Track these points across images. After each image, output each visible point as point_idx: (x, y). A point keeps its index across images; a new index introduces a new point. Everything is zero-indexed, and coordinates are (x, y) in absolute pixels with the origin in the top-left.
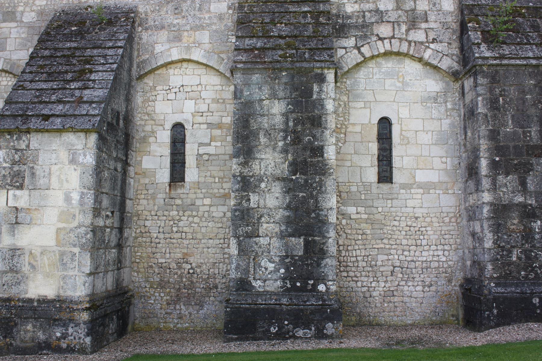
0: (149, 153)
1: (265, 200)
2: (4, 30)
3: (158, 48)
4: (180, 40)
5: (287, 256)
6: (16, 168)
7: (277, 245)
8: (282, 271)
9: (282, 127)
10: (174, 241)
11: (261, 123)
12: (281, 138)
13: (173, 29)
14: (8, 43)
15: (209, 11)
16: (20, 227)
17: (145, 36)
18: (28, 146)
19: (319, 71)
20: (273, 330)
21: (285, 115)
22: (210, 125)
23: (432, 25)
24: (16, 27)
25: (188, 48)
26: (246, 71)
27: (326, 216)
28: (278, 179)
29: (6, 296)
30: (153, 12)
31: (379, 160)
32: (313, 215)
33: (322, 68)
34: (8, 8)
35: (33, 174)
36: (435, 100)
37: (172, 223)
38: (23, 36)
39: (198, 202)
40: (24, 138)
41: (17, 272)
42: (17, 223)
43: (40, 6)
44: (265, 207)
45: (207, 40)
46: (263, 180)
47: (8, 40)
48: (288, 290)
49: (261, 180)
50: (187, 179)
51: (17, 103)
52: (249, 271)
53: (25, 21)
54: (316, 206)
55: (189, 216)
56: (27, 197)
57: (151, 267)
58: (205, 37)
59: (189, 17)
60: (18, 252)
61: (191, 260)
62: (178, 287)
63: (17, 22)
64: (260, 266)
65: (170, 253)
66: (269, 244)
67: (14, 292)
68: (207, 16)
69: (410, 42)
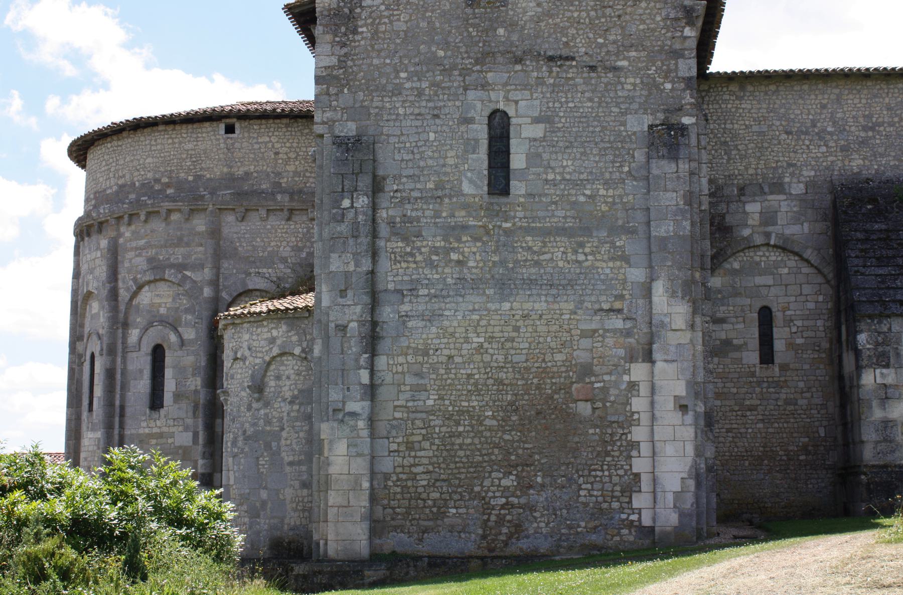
2: (773, 203)
6: (880, 349)
14: (779, 217)
16: (890, 401)
18: (890, 329)
24: (785, 200)
26: (688, 87)
29: (882, 463)
38: (795, 209)
40: (885, 322)
41: (891, 442)
42: (887, 398)
43: (809, 177)
47: (779, 214)
51: (864, 289)
53: (793, 192)
56: (893, 375)
60: (890, 424)
63: (785, 194)
67: (889, 458)
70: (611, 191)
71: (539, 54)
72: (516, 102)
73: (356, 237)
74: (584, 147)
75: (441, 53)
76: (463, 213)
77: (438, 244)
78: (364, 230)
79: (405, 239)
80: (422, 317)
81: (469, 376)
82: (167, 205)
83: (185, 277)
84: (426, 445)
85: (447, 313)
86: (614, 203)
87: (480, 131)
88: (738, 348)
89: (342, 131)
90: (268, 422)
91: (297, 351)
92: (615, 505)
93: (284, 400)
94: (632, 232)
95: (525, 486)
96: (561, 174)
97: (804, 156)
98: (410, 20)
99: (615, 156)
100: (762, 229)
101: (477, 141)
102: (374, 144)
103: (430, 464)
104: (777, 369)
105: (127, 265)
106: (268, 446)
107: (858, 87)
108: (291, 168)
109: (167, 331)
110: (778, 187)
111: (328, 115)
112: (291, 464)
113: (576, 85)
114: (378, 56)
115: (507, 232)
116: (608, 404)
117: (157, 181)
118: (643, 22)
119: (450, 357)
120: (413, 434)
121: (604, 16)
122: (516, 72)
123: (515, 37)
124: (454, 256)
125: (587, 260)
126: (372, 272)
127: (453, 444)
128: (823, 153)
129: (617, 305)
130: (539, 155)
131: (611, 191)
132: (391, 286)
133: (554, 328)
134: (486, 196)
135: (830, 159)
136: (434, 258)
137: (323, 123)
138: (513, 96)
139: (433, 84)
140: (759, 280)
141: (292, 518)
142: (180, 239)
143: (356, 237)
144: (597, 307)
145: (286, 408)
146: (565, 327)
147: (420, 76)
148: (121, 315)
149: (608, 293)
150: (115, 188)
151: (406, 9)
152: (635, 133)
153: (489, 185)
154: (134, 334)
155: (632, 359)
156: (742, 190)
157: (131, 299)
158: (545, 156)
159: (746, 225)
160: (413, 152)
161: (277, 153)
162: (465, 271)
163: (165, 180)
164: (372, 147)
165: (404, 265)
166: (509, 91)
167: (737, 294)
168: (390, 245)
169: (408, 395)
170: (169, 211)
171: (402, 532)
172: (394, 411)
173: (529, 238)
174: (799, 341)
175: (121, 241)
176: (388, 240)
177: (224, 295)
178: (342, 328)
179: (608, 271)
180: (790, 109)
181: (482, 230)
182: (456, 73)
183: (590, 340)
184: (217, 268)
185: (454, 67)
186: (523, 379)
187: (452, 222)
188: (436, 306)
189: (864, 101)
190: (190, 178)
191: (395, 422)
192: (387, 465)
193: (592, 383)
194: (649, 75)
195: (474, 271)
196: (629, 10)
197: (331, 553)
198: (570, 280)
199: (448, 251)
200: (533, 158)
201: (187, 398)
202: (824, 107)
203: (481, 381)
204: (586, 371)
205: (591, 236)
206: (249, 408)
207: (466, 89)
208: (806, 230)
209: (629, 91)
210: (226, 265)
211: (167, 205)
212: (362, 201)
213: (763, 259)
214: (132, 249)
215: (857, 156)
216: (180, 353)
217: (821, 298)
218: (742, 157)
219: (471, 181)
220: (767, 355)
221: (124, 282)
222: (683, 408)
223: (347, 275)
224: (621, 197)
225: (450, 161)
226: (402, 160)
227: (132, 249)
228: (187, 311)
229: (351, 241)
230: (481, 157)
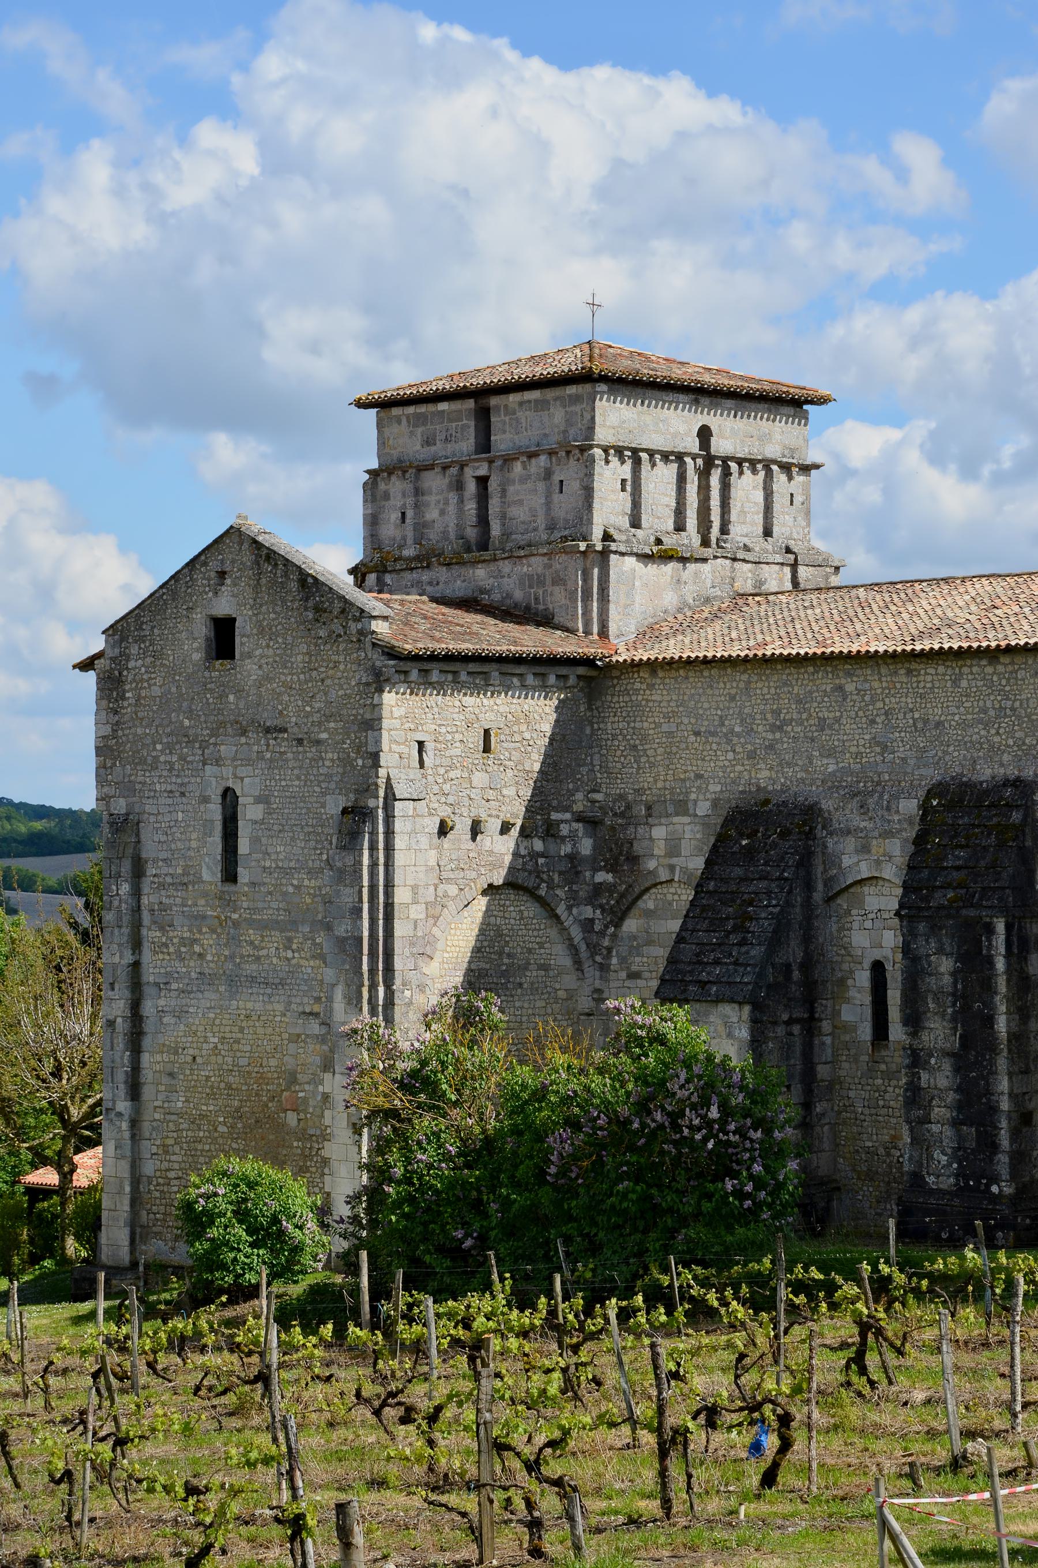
0: (848, 1000)
1: (935, 1079)
2: (678, 827)
3: (847, 861)
4: (869, 852)
5: (959, 1149)
7: (948, 1133)
8: (955, 1165)
9: (950, 989)
10: (881, 1119)
11: (929, 983)
12: (949, 1004)
13: (860, 835)
15: (897, 812)
17: (830, 842)
19: (988, 920)
20: (944, 1236)
21: (954, 974)
25: (878, 862)
27: (997, 1102)
28: (948, 1054)
30: (837, 809)
32: (984, 1100)
33: (991, 917)
34: (679, 794)
37: (877, 1094)
38: (698, 836)
43: (715, 793)
44: (936, 1088)
45: (897, 853)
46: (933, 1056)
47: (683, 841)
48: (961, 1189)
49: (931, 1055)
50: (891, 1038)
52: (922, 1164)
54: (987, 1090)
55: (895, 1087)
57: (857, 1151)
59: (877, 819)
62: (887, 1179)
64: (933, 1159)
65: (877, 1135)
66: (941, 1133)
68: (896, 818)
70: (313, 881)
71: (260, 725)
72: (242, 779)
73: (120, 927)
74: (293, 832)
75: (187, 722)
77: (185, 935)
79: (162, 929)
81: (208, 1078)
84: (177, 1149)
85: (191, 1010)
87: (215, 811)
89: (115, 809)
96: (276, 861)
97: (712, 765)
98: (164, 684)
99: (317, 842)
102: (138, 824)
103: (181, 1169)
107: (768, 672)
110: (682, 807)
113: (287, 760)
115: (236, 924)
116: (309, 1116)
120: (167, 1137)
122: (242, 745)
123: (241, 705)
125: (294, 957)
127: (196, 1150)
128: (730, 761)
129: (316, 1008)
131: (313, 881)
132: (151, 979)
134: (220, 884)
135: (739, 768)
136: (183, 949)
138: (242, 772)
143: (120, 927)
144: (301, 1009)
146: (277, 1030)
149: (309, 994)
151: (160, 671)
152: (332, 816)
158: (264, 840)
159: (652, 855)
160: (167, 834)
162: (205, 965)
165: (161, 956)
166: (236, 767)
168: (151, 934)
171: (161, 1239)
172: (155, 1111)
173: (251, 932)
176: (149, 929)
179: (309, 970)
180: (699, 701)
182: (197, 745)
183: (295, 1045)
186: (246, 1084)
188: (184, 1002)
189: (773, 691)
191: (155, 1124)
193: (297, 1092)
194: (344, 749)
195: (212, 965)
198: (281, 979)
200: (255, 841)
202: (733, 698)
203: (216, 1085)
205: (297, 931)
207: (204, 764)
209: (328, 767)
212: (125, 888)
213: (676, 897)
215: (763, 766)
218: (652, 765)
224: (320, 888)
225: (194, 844)
226: (159, 842)
229: (116, 930)
230: (216, 842)
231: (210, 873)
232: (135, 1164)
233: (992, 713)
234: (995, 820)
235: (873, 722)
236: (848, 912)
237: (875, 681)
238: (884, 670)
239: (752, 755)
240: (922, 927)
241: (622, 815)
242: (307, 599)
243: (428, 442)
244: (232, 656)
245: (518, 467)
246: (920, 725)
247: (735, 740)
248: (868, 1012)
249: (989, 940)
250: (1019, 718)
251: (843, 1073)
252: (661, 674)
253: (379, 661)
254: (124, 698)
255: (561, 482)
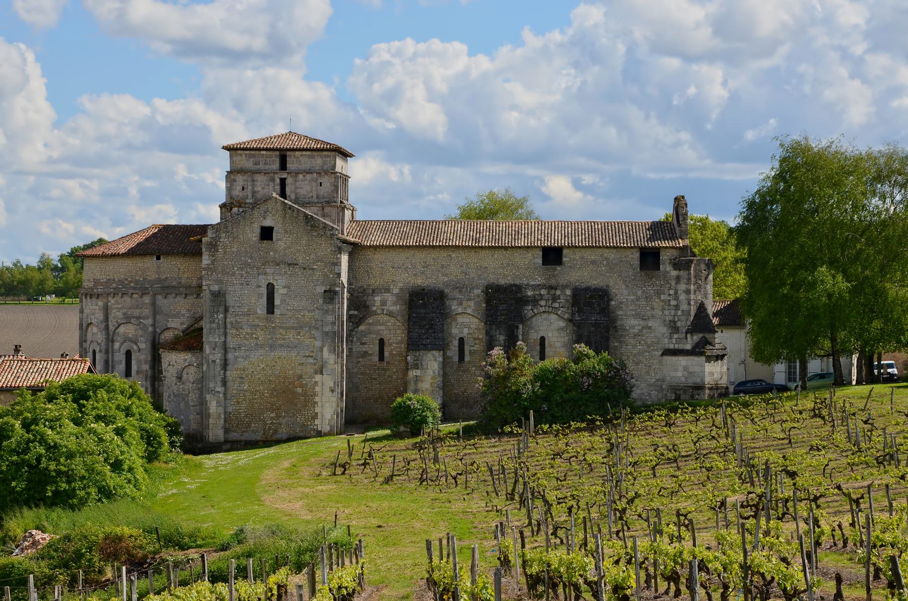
3: (453, 308)
4: (462, 305)
21: (505, 340)
22: (474, 339)
23: (562, 301)
25: (465, 308)
31: (540, 353)
35: (422, 364)
36: (562, 329)
39: (470, 369)
45: (473, 305)
50: (465, 360)
58: (472, 303)
61: (468, 391)
69: (553, 308)
72: (277, 280)
73: (219, 329)
75: (250, 261)
76: (257, 320)
78: (222, 326)
79: (237, 329)
80: (243, 357)
82: (132, 291)
83: (141, 322)
86: (311, 318)
87: (264, 291)
88: (370, 355)
90: (184, 390)
91: (195, 364)
92: (309, 423)
93: (190, 382)
94: (317, 329)
95: (278, 417)
100: (381, 307)
101: (262, 294)
104: (385, 364)
105: (113, 315)
106: (184, 399)
108: (186, 276)
109: (133, 344)
110: (388, 290)
111: (208, 282)
112: (193, 406)
114: (226, 261)
115: (273, 328)
117: (126, 279)
118: (323, 252)
119: (253, 372)
121: (309, 249)
124: (254, 336)
126: (225, 341)
129: (311, 354)
130: (285, 300)
132: (231, 346)
133: (290, 362)
137: (206, 285)
139: (247, 272)
140: (380, 328)
141: (194, 426)
142: (138, 306)
143: (219, 329)
145: (191, 385)
147: (242, 269)
148: (111, 337)
150: (105, 280)
153: (267, 310)
154: (117, 345)
155: (316, 373)
156: (373, 291)
157: (115, 330)
158: (287, 300)
161: (179, 269)
163: (130, 279)
164: (224, 295)
165: (236, 339)
167: (370, 333)
168: (231, 331)
169: (238, 385)
170: (132, 294)
174: (394, 352)
175: (109, 304)
176: (230, 329)
177: (158, 330)
178: (214, 361)
181: (264, 327)
184: (155, 319)
185: (254, 266)
187: (254, 323)
190: (141, 279)
192: (230, 409)
196: (318, 247)
197: (211, 440)
199: (252, 334)
200: (283, 301)
201: (142, 373)
202: (408, 258)
204: (300, 377)
206: (176, 384)
207: (259, 275)
208: (398, 309)
210: (158, 317)
211: (132, 291)
212: (221, 316)
214: (115, 308)
216: (138, 354)
217: (403, 336)
218: (374, 277)
219: (260, 309)
220: (381, 357)
221: (111, 322)
222: (333, 391)
223: (216, 343)
227: (115, 308)
228: (141, 336)
229: (217, 330)
230: (264, 300)
231: (261, 310)
232: (225, 407)
233: (505, 265)
234: (512, 296)
235: (462, 266)
236: (451, 323)
237: (463, 254)
238: (466, 251)
239: (415, 275)
240: (494, 327)
241: (362, 293)
242: (308, 223)
243: (256, 164)
244: (271, 239)
245: (301, 176)
246: (479, 268)
247: (409, 270)
248: (457, 353)
249: (517, 330)
250: (514, 267)
251: (447, 371)
252: (378, 250)
253: (340, 244)
254: (218, 251)
255: (321, 183)
